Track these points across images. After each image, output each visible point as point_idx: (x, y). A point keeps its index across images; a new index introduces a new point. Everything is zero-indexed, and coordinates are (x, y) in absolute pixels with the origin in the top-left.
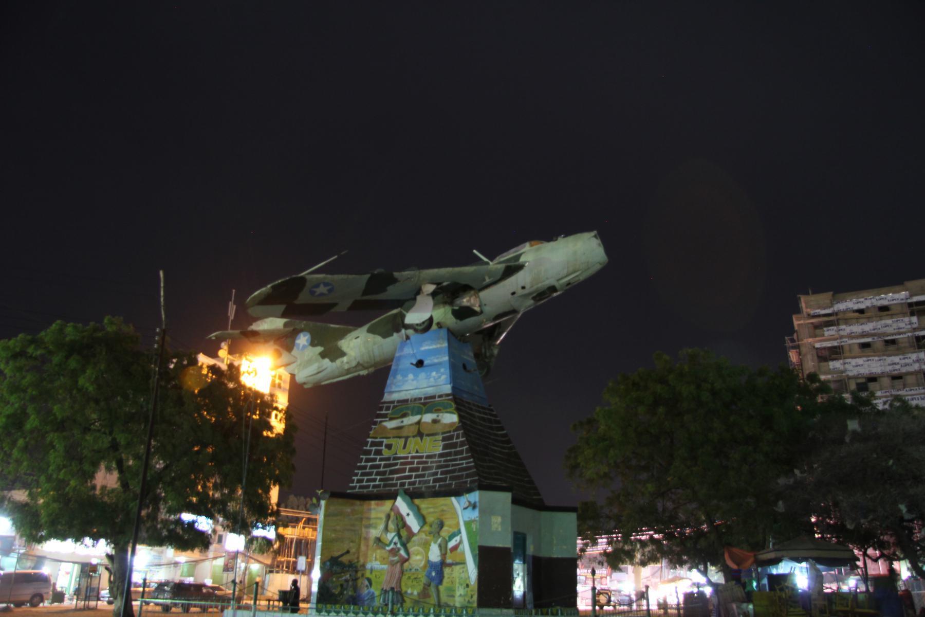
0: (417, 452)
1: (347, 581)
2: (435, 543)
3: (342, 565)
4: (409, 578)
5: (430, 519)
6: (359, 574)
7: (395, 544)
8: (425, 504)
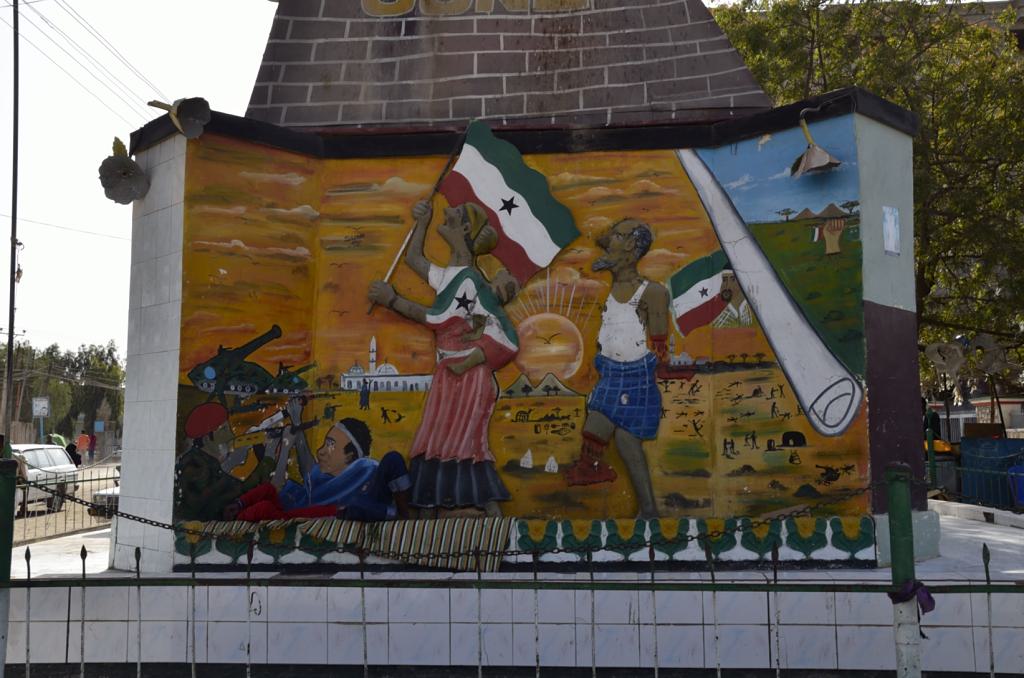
0: (499, 9)
1: (275, 433)
2: (623, 299)
3: (256, 377)
4: (522, 416)
5: (597, 221)
6: (318, 407)
7: (464, 302)
8: (562, 173)
